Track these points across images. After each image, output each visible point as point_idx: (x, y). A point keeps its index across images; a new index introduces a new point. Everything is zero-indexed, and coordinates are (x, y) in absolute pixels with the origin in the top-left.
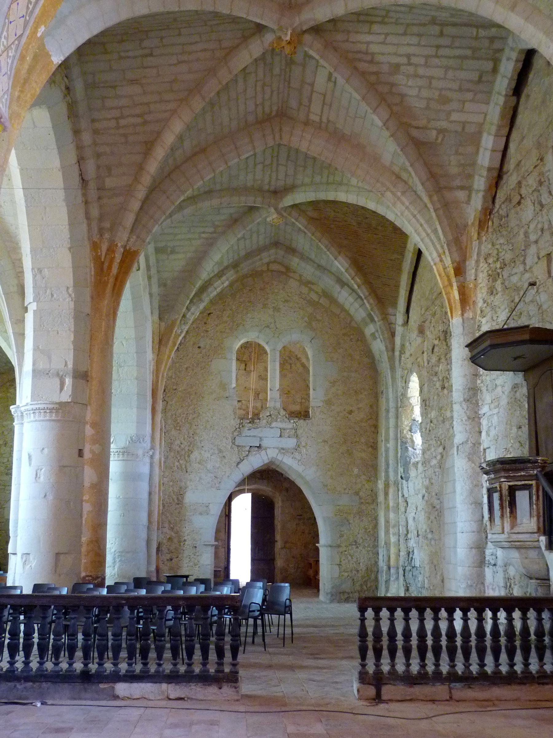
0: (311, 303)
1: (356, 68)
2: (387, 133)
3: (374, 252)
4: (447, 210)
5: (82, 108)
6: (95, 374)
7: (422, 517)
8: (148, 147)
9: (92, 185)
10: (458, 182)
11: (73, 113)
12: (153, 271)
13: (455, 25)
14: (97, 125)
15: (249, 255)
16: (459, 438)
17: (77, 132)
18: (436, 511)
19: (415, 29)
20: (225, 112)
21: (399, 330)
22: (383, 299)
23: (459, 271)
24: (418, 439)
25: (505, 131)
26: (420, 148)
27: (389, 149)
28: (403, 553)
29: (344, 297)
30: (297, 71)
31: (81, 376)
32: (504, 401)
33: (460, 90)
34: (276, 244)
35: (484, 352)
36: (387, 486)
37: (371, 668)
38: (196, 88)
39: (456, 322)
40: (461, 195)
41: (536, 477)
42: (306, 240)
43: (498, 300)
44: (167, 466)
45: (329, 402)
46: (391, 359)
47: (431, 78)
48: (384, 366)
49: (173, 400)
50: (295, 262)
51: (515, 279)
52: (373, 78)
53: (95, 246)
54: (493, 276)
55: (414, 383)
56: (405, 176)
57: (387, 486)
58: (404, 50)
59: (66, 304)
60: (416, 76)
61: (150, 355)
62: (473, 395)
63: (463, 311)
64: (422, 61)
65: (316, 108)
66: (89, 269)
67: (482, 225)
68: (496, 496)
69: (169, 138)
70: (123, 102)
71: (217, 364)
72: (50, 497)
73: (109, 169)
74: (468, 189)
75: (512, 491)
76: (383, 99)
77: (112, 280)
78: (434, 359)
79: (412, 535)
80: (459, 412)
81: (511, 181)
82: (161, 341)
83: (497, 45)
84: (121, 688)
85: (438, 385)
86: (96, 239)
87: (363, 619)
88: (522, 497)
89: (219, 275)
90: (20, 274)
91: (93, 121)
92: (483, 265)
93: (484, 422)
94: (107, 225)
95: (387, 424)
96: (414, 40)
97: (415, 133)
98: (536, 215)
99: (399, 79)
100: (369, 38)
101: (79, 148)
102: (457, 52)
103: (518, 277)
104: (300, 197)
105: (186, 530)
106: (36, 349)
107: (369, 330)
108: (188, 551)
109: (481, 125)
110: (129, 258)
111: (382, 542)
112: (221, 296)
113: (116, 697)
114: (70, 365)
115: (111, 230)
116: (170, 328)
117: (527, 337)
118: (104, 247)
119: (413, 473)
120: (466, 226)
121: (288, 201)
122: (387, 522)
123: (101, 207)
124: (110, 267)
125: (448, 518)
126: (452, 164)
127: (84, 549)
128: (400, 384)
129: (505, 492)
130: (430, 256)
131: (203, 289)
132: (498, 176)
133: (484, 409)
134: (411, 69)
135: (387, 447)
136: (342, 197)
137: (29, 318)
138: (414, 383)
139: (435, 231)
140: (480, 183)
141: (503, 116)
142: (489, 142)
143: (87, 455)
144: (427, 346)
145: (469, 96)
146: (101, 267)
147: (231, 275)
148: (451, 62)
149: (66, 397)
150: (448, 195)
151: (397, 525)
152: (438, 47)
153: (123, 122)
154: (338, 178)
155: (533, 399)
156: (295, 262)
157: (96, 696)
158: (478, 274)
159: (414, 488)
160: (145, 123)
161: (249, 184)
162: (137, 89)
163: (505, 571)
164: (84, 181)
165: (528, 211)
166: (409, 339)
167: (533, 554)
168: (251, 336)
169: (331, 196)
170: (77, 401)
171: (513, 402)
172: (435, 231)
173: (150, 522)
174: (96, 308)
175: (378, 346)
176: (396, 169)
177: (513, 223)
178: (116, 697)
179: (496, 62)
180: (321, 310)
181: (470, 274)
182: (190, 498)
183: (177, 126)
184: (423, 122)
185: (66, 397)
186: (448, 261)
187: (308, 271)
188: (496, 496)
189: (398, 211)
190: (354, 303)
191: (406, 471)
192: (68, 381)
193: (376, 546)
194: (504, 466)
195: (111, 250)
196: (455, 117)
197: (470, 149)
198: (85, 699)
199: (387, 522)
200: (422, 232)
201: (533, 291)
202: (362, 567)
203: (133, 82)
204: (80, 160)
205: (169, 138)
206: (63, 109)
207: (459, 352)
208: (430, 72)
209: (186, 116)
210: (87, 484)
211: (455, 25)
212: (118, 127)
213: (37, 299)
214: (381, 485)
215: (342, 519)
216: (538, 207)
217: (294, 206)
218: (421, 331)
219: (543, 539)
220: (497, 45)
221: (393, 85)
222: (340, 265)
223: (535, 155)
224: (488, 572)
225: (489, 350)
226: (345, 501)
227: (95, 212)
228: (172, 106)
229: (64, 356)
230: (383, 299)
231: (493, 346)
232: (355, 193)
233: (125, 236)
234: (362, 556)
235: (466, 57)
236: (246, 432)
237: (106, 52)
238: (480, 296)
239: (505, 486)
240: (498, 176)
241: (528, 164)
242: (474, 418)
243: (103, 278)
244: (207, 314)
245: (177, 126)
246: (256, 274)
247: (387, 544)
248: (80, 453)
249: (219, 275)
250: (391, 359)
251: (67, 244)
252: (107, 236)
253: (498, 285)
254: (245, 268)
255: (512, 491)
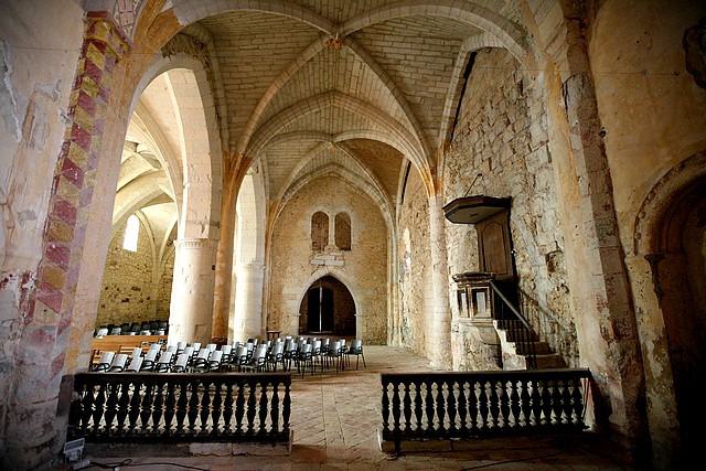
0: (352, 193)
1: (375, 61)
2: (392, 97)
3: (384, 166)
4: (427, 140)
5: (217, 76)
6: (223, 223)
7: (412, 302)
8: (258, 101)
9: (224, 122)
10: (432, 126)
11: (210, 77)
12: (266, 174)
13: (431, 37)
14: (227, 87)
15: (318, 169)
16: (435, 261)
17: (214, 90)
18: (420, 299)
19: (410, 40)
20: (302, 85)
21: (398, 207)
22: (389, 192)
23: (434, 172)
24: (408, 261)
25: (459, 97)
26: (410, 106)
27: (393, 107)
28: (401, 320)
29: (368, 190)
30: (342, 64)
31: (215, 224)
32: (462, 240)
33: (434, 75)
34: (333, 163)
35: (454, 211)
36: (392, 285)
37: (391, 427)
38: (285, 69)
39: (432, 199)
40: (434, 132)
41: (489, 285)
42: (349, 161)
43: (456, 186)
44: (272, 274)
45: (361, 243)
46: (394, 221)
47: (417, 68)
48: (390, 224)
49: (273, 241)
50: (343, 172)
51: (467, 174)
52: (385, 67)
53: (225, 153)
54: (454, 174)
55: (407, 233)
56: (402, 122)
57: (392, 285)
58: (402, 51)
59: (206, 185)
60: (409, 65)
61: (264, 217)
62: (442, 239)
63: (436, 192)
64: (413, 58)
65: (353, 85)
66: (221, 167)
67: (446, 148)
68: (463, 295)
69: (269, 96)
70: (244, 75)
71: (301, 223)
72: (193, 292)
73: (235, 112)
74: (439, 129)
75: (474, 292)
76: (391, 78)
77: (235, 172)
78: (418, 220)
79: (406, 311)
80: (434, 247)
81: (463, 122)
82: (270, 210)
83: (455, 50)
84: (195, 447)
85: (421, 234)
86: (227, 149)
87: (385, 391)
88: (481, 297)
89: (303, 177)
90: (181, 169)
91: (225, 85)
92: (447, 168)
93: (449, 252)
94: (233, 143)
95: (392, 254)
96: (409, 46)
97: (408, 98)
98: (479, 138)
99: (400, 68)
100: (383, 44)
101: (216, 98)
102: (434, 54)
103: (468, 173)
104: (345, 137)
105: (283, 308)
106: (189, 209)
107: (382, 207)
108: (284, 319)
109: (445, 95)
110: (246, 163)
111: (389, 314)
112: (304, 188)
113: (190, 454)
114: (209, 218)
115: (236, 146)
116: (275, 203)
117: (481, 202)
118: (232, 154)
119: (406, 279)
120: (436, 149)
121: (339, 139)
122: (392, 304)
123: (230, 133)
124: (234, 166)
125: (427, 303)
126: (429, 115)
127: (214, 323)
128: (398, 234)
129: (470, 293)
130: (416, 164)
131: (294, 185)
132: (454, 123)
133: (449, 246)
134: (407, 62)
135: (392, 266)
136: (368, 136)
137: (185, 191)
138: (407, 233)
139: (420, 151)
140: (445, 125)
141: (457, 89)
142: (449, 103)
143: (217, 268)
144: (414, 214)
145: (439, 78)
146: (229, 165)
147: (309, 178)
148: (430, 59)
149: (205, 235)
150: (427, 132)
151: (397, 306)
152: (422, 50)
153: (242, 87)
154: (365, 127)
155: (481, 238)
156: (343, 172)
157: (173, 454)
158: (445, 174)
159: (407, 286)
160: (256, 88)
161: (318, 129)
162: (250, 68)
163: (464, 336)
164: (219, 118)
165: (475, 137)
166: (403, 211)
167: (488, 330)
168: (320, 209)
169: (362, 136)
170: (213, 238)
171: (468, 241)
172: (420, 151)
173: (263, 303)
174: (225, 188)
175: (387, 215)
176: (398, 119)
177: (465, 144)
178: (190, 454)
179: (454, 60)
180: (357, 196)
181: (440, 174)
182: (285, 291)
183: (274, 90)
184: (412, 93)
185: (205, 235)
186: (427, 167)
187: (350, 177)
188: (463, 295)
189: (396, 142)
190: (374, 193)
191: (402, 277)
192: (207, 227)
193: (386, 316)
194: (461, 278)
195: (236, 156)
196: (431, 90)
197: (440, 107)
198: (166, 456)
199: (392, 304)
200: (412, 154)
201: (480, 179)
202: (379, 327)
203: (247, 64)
204: (217, 106)
205: (269, 96)
206: (204, 73)
207: (434, 212)
208: (416, 64)
209: (280, 84)
210: (217, 284)
211: (431, 37)
212: (239, 89)
213: (190, 181)
214: (389, 285)
215: (368, 302)
216: (481, 133)
217: (342, 142)
218: (410, 206)
219: (495, 322)
220: (455, 50)
221: (396, 71)
222: (366, 173)
223: (478, 107)
224: (453, 335)
225: (454, 211)
226: (369, 293)
227: (226, 135)
228: (271, 79)
229: (205, 212)
230: (389, 192)
231: (460, 208)
232: (377, 133)
233: (244, 150)
234: (379, 321)
235: (437, 56)
236: (316, 257)
237: (230, 46)
238: (446, 185)
239: (470, 289)
240: (454, 123)
241: (475, 112)
242: (444, 250)
243: (229, 174)
244: (296, 197)
245: (274, 90)
246: (322, 178)
247: (392, 315)
248: (214, 268)
249: (303, 177)
250: (394, 221)
251: (208, 151)
252: (233, 149)
253: (457, 178)
254: (316, 175)
255: (474, 292)
